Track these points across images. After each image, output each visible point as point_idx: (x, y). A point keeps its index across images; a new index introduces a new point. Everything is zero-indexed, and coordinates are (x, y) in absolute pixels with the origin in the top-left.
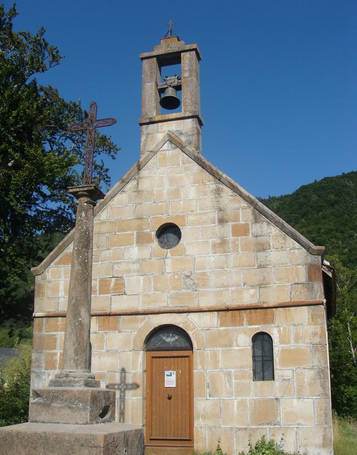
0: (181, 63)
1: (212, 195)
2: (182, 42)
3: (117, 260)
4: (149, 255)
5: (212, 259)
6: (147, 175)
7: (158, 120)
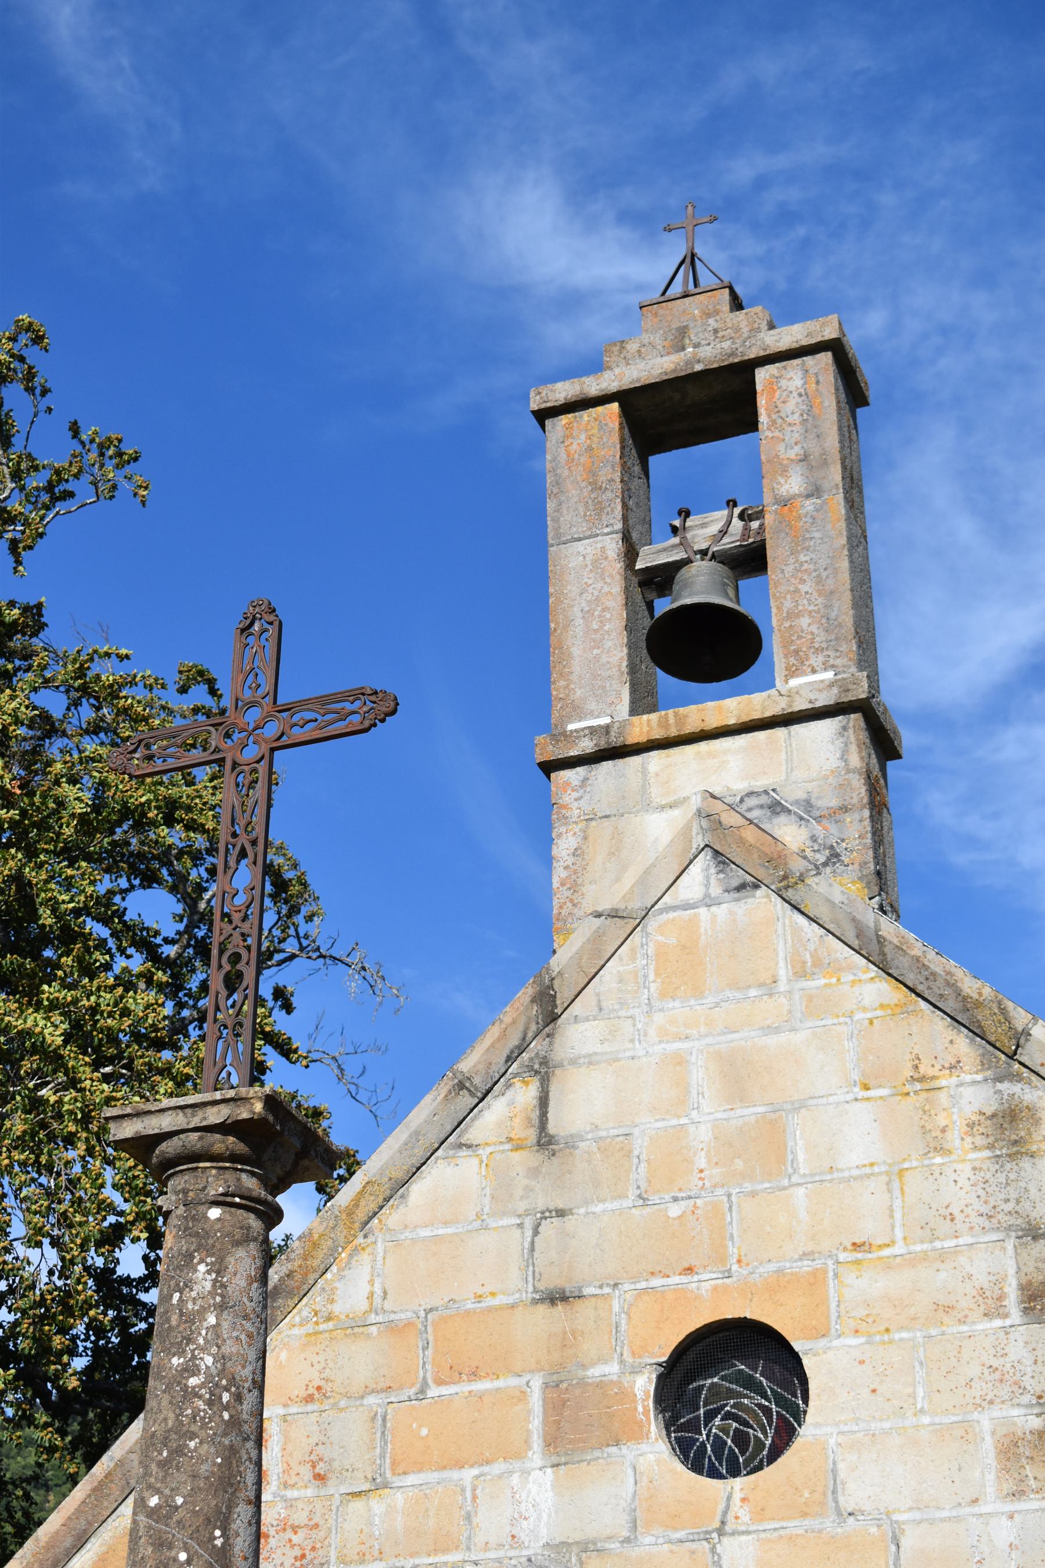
0: (752, 425)
1: (976, 1148)
2: (756, 313)
3: (436, 1551)
4: (624, 1519)
5: (1003, 1532)
6: (589, 1048)
7: (643, 739)
